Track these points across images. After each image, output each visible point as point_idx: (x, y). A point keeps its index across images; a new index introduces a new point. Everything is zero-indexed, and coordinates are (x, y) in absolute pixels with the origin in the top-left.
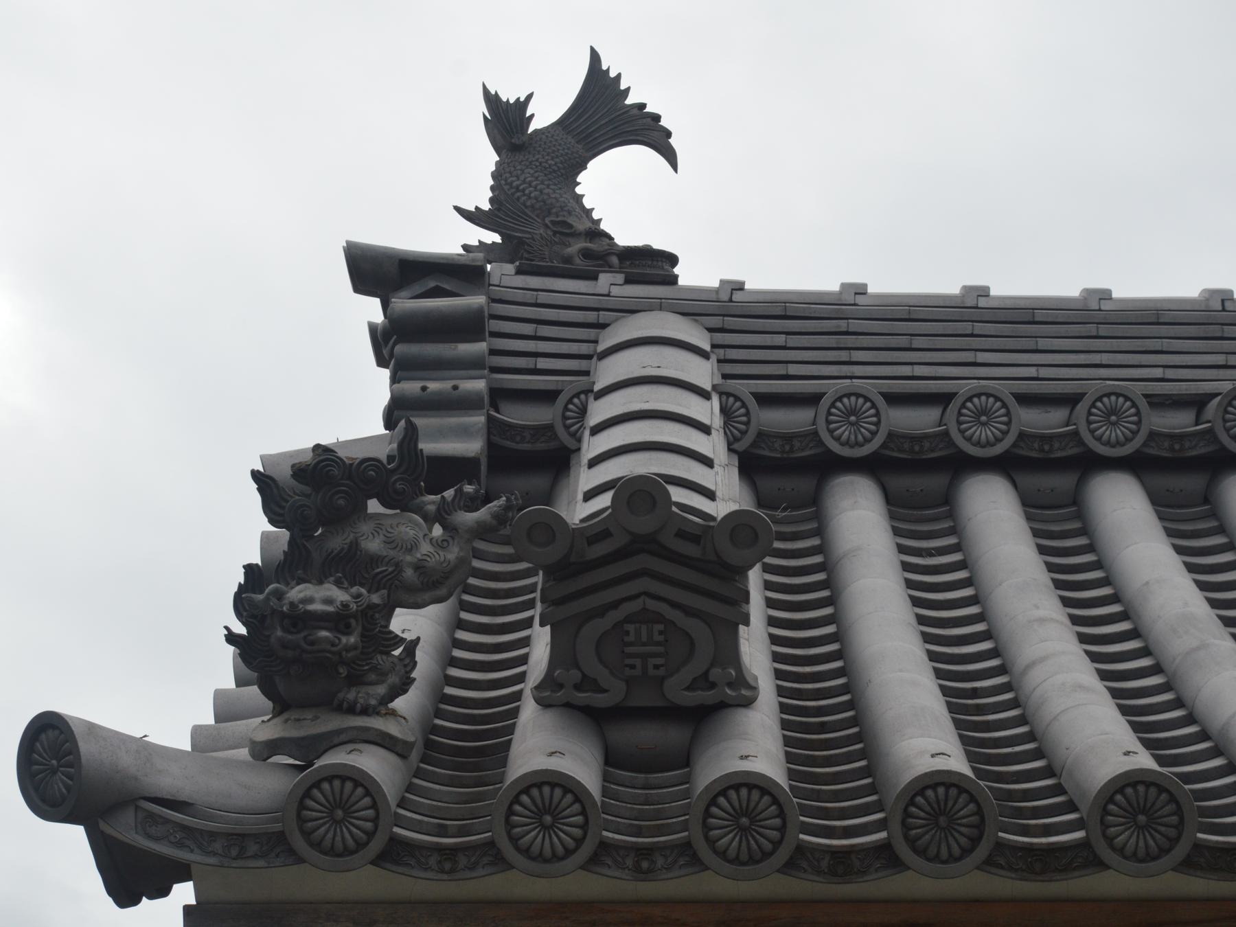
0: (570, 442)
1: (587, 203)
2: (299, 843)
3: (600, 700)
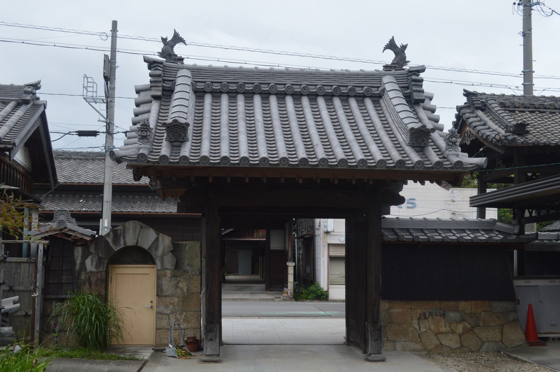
0: (173, 89)
1: (174, 50)
2: (454, 168)
3: (171, 140)
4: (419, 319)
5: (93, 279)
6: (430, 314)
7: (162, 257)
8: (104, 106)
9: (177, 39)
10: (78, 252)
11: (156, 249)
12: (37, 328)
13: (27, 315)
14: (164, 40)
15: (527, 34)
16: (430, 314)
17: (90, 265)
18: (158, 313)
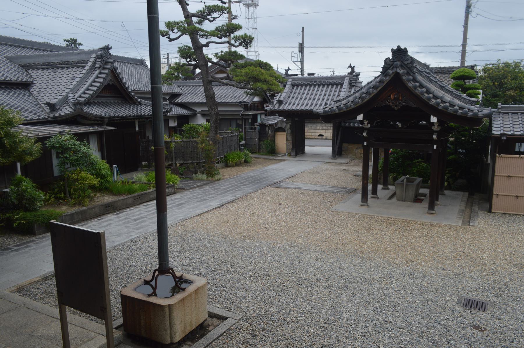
4: (356, 149)
5: (271, 136)
6: (360, 148)
7: (288, 129)
8: (300, 63)
9: (289, 69)
10: (267, 128)
11: (286, 128)
12: (257, 148)
13: (255, 144)
14: (286, 70)
15: (466, 27)
16: (360, 148)
17: (270, 132)
18: (287, 145)
